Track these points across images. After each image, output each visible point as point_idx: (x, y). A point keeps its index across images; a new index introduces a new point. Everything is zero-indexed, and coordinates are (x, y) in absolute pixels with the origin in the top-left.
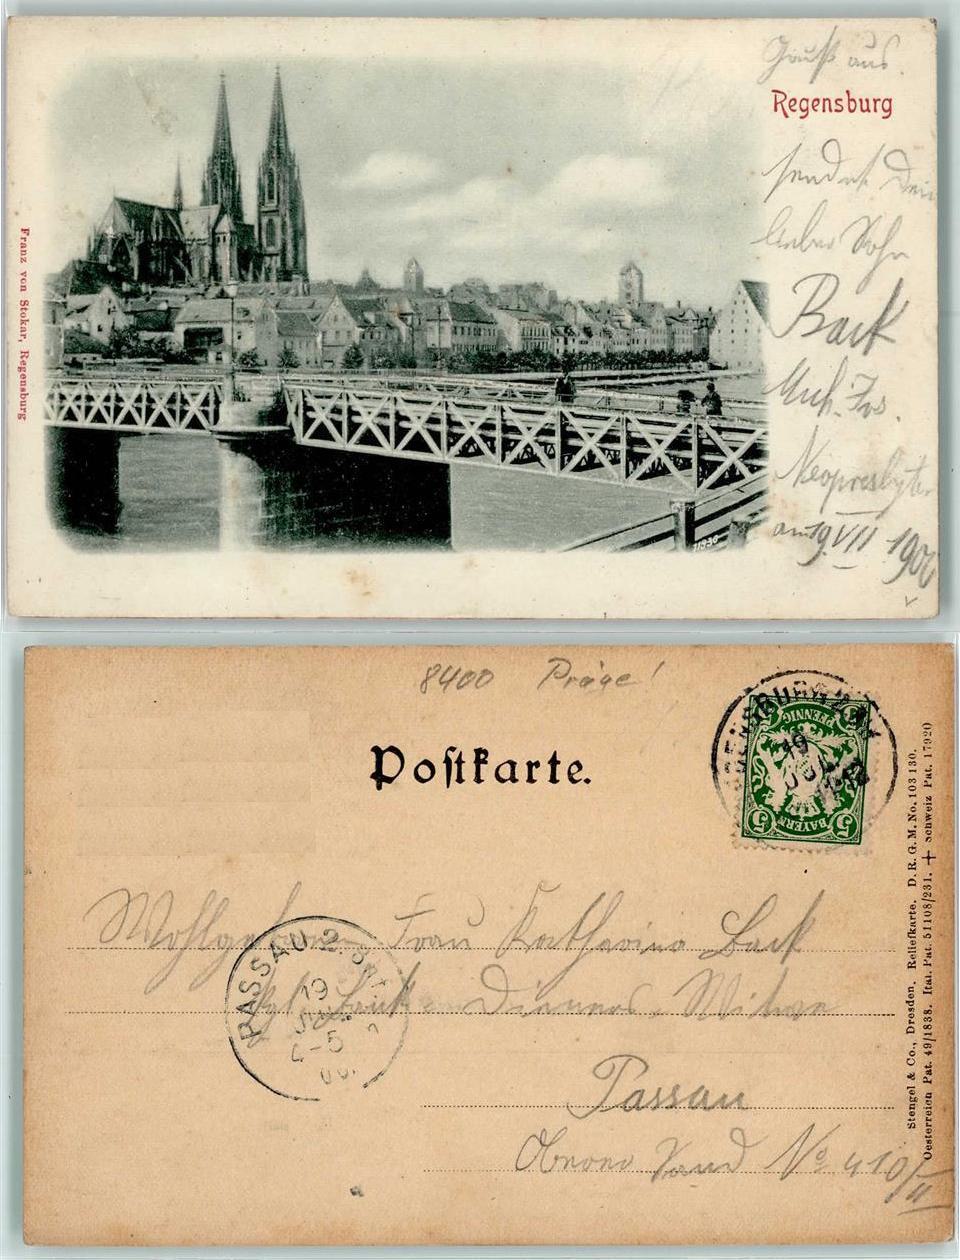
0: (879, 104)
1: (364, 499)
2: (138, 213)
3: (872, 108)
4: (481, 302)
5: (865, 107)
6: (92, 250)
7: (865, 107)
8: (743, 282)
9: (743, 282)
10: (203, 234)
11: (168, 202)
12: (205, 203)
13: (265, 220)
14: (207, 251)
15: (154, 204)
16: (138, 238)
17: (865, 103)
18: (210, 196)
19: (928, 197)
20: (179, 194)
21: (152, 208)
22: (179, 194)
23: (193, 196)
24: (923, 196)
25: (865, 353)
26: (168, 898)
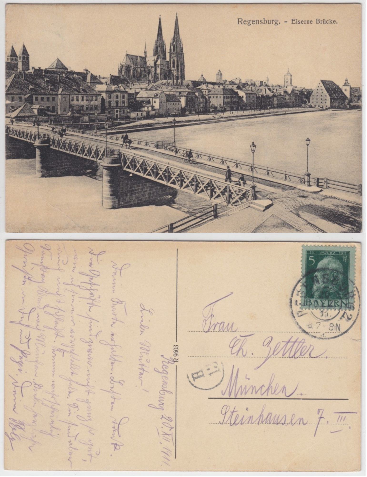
0: (274, 21)
1: (122, 203)
2: (131, 58)
3: (271, 23)
4: (235, 88)
5: (269, 23)
6: (120, 69)
7: (269, 23)
8: (321, 80)
9: (321, 80)
10: (152, 64)
11: (143, 55)
12: (154, 55)
13: (172, 60)
14: (153, 69)
15: (137, 55)
16: (133, 66)
17: (269, 21)
18: (156, 52)
19: (88, 378)
20: (145, 53)
21: (137, 57)
22: (145, 53)
23: (150, 53)
24: (88, 355)
25: (222, 391)
26: (61, 376)
